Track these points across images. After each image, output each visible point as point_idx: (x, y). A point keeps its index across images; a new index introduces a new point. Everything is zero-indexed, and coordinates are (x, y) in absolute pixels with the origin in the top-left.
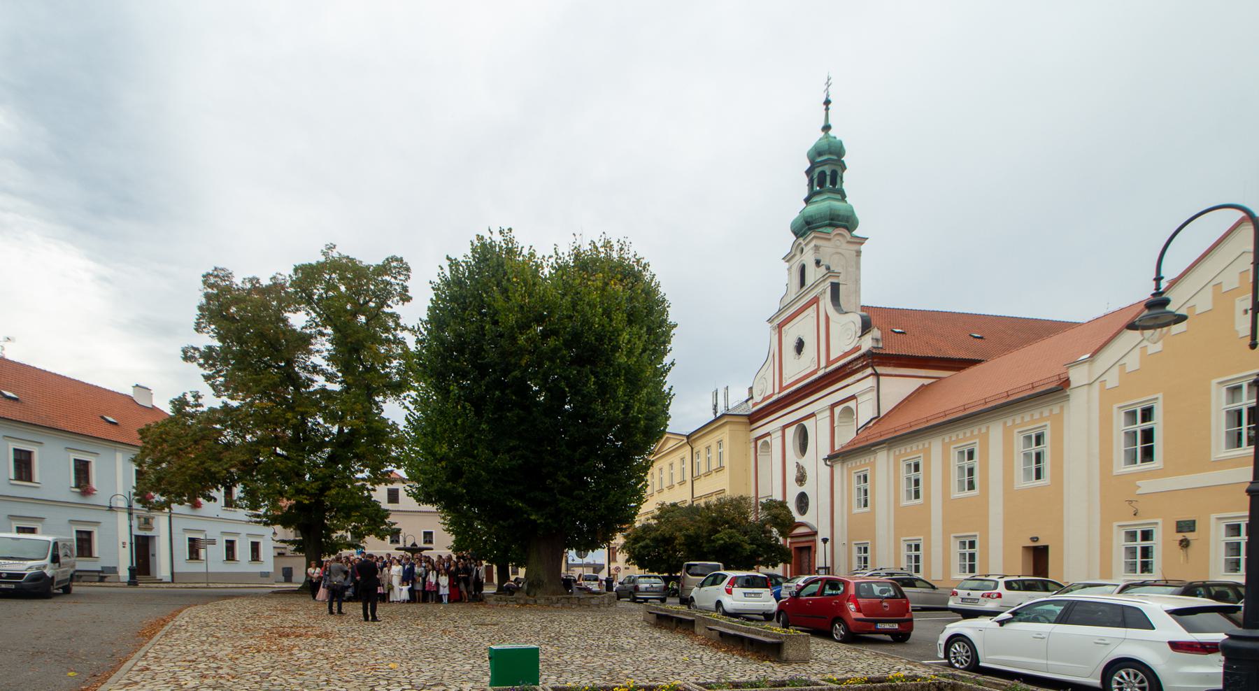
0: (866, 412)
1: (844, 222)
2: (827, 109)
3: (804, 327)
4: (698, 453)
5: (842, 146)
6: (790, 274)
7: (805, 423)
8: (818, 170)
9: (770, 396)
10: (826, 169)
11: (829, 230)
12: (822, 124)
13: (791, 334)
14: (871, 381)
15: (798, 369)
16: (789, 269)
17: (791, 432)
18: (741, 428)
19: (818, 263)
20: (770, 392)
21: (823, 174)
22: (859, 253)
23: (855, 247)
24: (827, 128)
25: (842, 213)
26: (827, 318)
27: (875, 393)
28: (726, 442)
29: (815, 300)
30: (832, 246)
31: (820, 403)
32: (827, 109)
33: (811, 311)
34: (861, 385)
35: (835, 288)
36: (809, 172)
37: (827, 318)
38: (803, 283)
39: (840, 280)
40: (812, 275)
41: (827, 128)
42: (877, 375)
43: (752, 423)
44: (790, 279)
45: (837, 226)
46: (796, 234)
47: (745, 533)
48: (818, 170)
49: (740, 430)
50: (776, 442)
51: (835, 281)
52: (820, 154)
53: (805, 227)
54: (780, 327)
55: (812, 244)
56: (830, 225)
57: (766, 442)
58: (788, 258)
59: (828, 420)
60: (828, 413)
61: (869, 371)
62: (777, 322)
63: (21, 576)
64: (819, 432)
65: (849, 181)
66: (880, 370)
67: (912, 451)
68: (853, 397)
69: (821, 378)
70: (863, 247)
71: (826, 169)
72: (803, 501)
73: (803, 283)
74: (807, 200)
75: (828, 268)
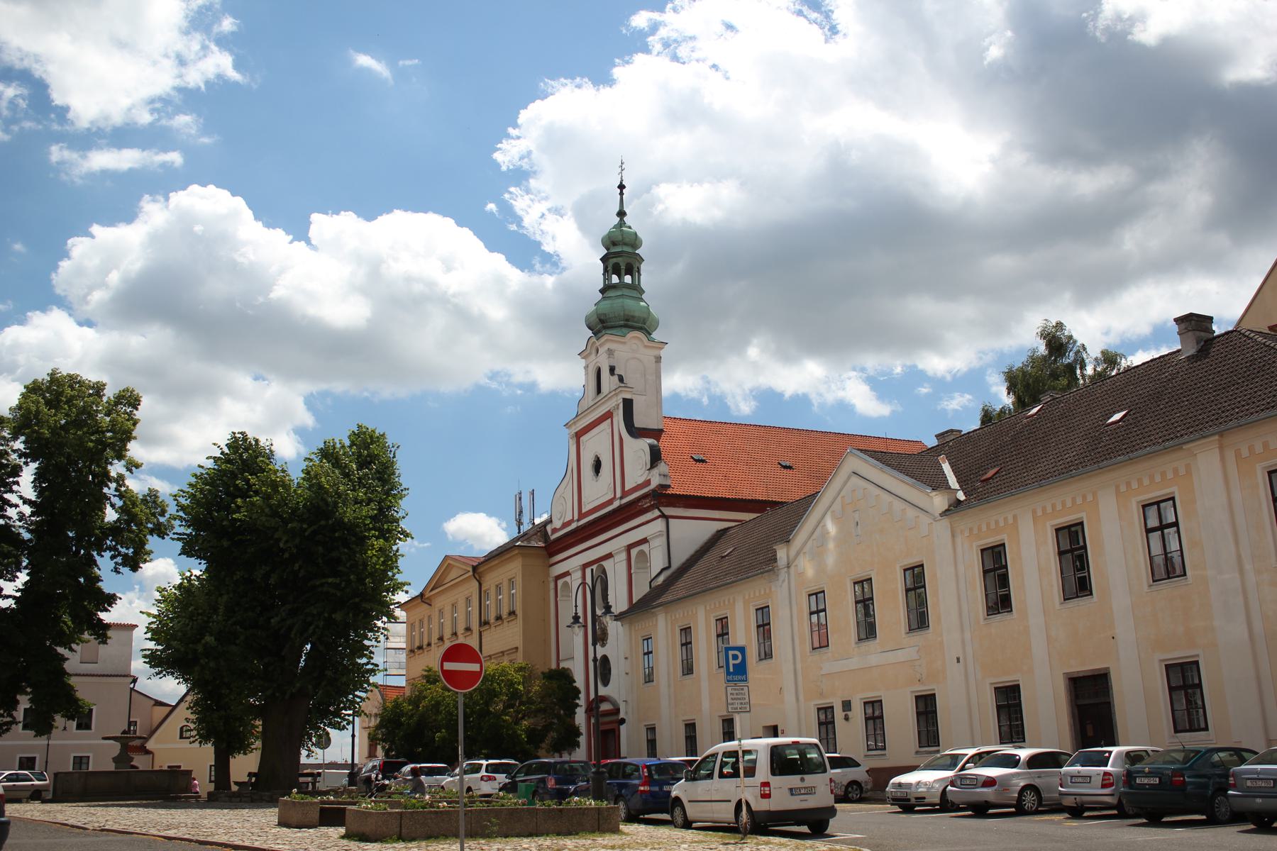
1: (640, 324)
2: (622, 194)
3: (598, 443)
6: (587, 374)
7: (604, 563)
9: (569, 523)
14: (659, 525)
15: (598, 492)
16: (586, 367)
19: (612, 370)
20: (569, 518)
23: (656, 352)
24: (621, 214)
25: (637, 314)
27: (664, 538)
28: (519, 581)
29: (609, 415)
30: (626, 348)
31: (615, 543)
32: (622, 194)
33: (605, 425)
34: (650, 527)
38: (599, 391)
40: (608, 382)
41: (621, 214)
42: (663, 516)
43: (551, 555)
44: (587, 380)
47: (121, 496)
51: (628, 396)
52: (614, 244)
53: (601, 324)
54: (578, 436)
55: (605, 348)
56: (626, 326)
57: (642, 553)
59: (624, 565)
60: (624, 556)
66: (668, 511)
68: (644, 541)
69: (621, 508)
70: (663, 353)
72: (603, 669)
73: (599, 391)
75: (621, 379)
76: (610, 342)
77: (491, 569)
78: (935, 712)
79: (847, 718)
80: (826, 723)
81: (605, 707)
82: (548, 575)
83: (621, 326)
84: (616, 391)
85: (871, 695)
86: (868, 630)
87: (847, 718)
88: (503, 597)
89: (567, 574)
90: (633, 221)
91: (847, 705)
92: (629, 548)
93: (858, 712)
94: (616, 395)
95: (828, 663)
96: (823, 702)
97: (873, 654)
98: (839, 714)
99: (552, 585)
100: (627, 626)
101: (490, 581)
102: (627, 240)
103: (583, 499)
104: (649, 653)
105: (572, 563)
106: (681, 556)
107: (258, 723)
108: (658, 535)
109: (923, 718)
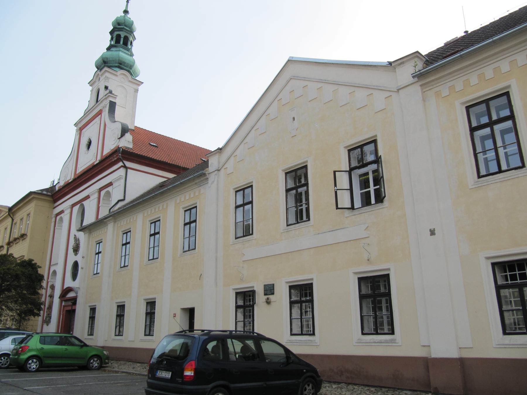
0: (116, 194)
1: (126, 67)
4: (15, 224)
5: (133, 22)
6: (91, 94)
8: (116, 33)
10: (122, 34)
11: (117, 69)
12: (124, 9)
13: (88, 133)
14: (122, 171)
15: (88, 159)
16: (92, 91)
17: (76, 209)
18: (46, 204)
19: (106, 88)
21: (119, 36)
22: (137, 91)
23: (135, 86)
24: (126, 12)
25: (127, 61)
26: (105, 125)
29: (100, 113)
30: (115, 80)
33: (97, 120)
34: (115, 174)
35: (112, 106)
36: (111, 33)
37: (105, 125)
39: (117, 101)
43: (55, 201)
45: (122, 69)
46: (97, 67)
48: (116, 33)
49: (44, 205)
50: (66, 217)
53: (104, 64)
55: (104, 76)
58: (91, 83)
59: (69, 215)
61: (121, 164)
62: (80, 125)
63: (388, 321)
64: (90, 207)
65: (136, 47)
66: (128, 164)
67: (124, 223)
68: (110, 184)
71: (122, 34)
74: (108, 49)
76: (108, 73)
77: (19, 209)
78: (388, 295)
79: (268, 302)
80: (246, 301)
81: (71, 295)
82: (52, 213)
83: (116, 67)
84: (106, 97)
85: (300, 278)
86: (300, 213)
87: (268, 302)
88: (23, 227)
89: (62, 212)
90: (131, 16)
91: (269, 290)
92: (101, 189)
93: (282, 296)
94: (106, 99)
95: (251, 248)
96: (244, 286)
97: (305, 235)
98: (260, 298)
99: (53, 220)
100: (87, 235)
101: (18, 217)
102: (127, 23)
103: (78, 166)
104: (99, 253)
105: (65, 204)
106: (132, 195)
107: (189, 373)
108: (119, 178)
109: (368, 304)
